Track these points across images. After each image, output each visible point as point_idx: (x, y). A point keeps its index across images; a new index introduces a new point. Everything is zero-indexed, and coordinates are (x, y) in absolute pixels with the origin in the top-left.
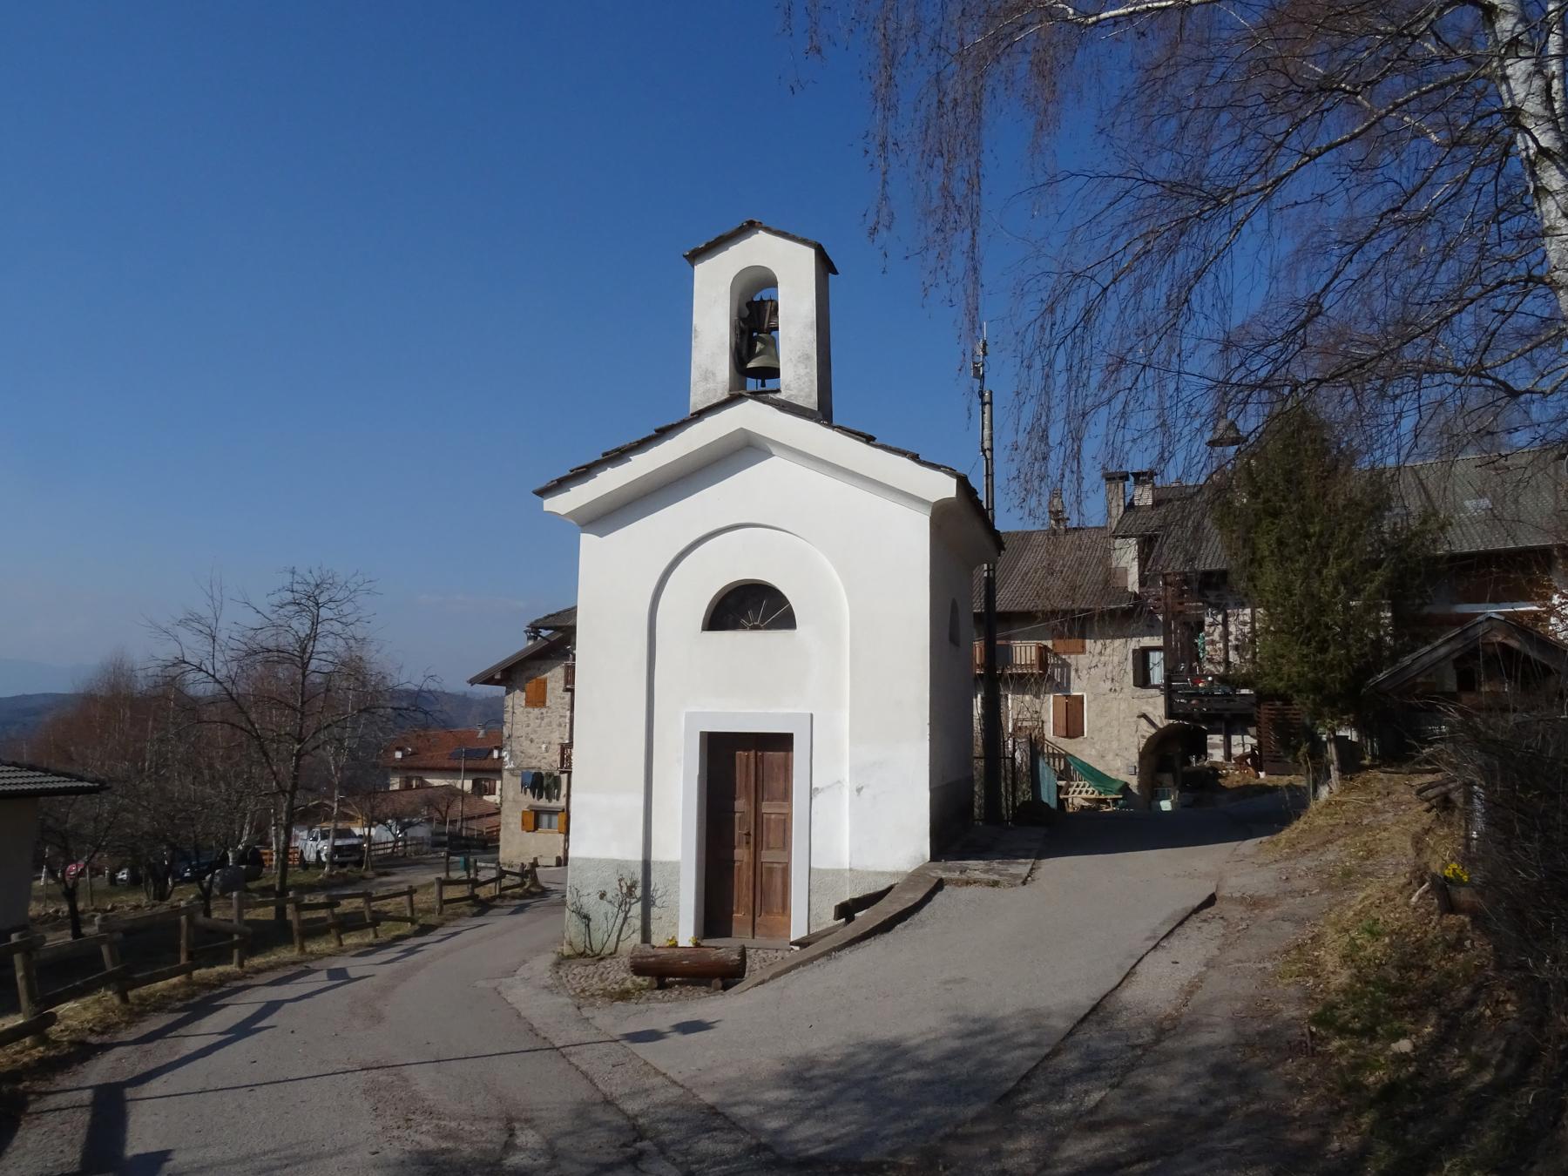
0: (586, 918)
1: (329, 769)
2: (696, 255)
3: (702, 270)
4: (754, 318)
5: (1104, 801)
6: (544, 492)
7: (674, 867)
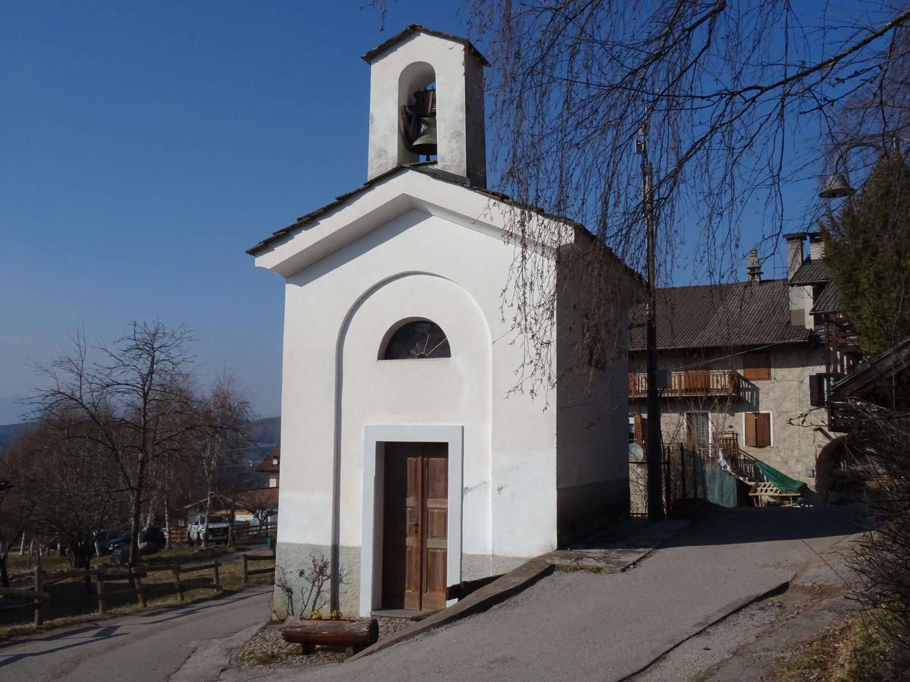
0: (289, 591)
1: (203, 471)
2: (373, 56)
3: (377, 68)
4: (418, 108)
5: (787, 498)
6: (256, 252)
7: (357, 550)
